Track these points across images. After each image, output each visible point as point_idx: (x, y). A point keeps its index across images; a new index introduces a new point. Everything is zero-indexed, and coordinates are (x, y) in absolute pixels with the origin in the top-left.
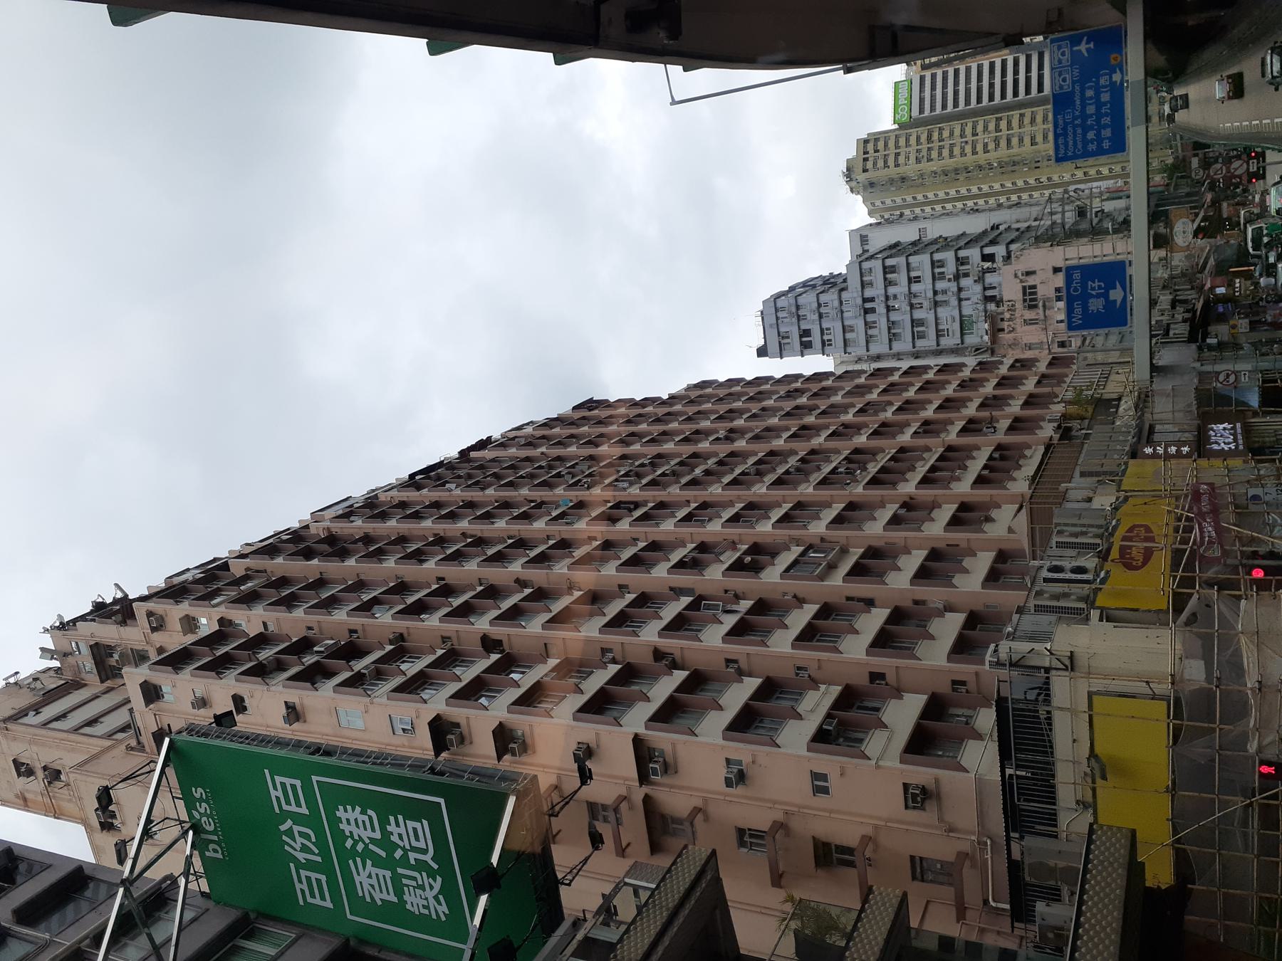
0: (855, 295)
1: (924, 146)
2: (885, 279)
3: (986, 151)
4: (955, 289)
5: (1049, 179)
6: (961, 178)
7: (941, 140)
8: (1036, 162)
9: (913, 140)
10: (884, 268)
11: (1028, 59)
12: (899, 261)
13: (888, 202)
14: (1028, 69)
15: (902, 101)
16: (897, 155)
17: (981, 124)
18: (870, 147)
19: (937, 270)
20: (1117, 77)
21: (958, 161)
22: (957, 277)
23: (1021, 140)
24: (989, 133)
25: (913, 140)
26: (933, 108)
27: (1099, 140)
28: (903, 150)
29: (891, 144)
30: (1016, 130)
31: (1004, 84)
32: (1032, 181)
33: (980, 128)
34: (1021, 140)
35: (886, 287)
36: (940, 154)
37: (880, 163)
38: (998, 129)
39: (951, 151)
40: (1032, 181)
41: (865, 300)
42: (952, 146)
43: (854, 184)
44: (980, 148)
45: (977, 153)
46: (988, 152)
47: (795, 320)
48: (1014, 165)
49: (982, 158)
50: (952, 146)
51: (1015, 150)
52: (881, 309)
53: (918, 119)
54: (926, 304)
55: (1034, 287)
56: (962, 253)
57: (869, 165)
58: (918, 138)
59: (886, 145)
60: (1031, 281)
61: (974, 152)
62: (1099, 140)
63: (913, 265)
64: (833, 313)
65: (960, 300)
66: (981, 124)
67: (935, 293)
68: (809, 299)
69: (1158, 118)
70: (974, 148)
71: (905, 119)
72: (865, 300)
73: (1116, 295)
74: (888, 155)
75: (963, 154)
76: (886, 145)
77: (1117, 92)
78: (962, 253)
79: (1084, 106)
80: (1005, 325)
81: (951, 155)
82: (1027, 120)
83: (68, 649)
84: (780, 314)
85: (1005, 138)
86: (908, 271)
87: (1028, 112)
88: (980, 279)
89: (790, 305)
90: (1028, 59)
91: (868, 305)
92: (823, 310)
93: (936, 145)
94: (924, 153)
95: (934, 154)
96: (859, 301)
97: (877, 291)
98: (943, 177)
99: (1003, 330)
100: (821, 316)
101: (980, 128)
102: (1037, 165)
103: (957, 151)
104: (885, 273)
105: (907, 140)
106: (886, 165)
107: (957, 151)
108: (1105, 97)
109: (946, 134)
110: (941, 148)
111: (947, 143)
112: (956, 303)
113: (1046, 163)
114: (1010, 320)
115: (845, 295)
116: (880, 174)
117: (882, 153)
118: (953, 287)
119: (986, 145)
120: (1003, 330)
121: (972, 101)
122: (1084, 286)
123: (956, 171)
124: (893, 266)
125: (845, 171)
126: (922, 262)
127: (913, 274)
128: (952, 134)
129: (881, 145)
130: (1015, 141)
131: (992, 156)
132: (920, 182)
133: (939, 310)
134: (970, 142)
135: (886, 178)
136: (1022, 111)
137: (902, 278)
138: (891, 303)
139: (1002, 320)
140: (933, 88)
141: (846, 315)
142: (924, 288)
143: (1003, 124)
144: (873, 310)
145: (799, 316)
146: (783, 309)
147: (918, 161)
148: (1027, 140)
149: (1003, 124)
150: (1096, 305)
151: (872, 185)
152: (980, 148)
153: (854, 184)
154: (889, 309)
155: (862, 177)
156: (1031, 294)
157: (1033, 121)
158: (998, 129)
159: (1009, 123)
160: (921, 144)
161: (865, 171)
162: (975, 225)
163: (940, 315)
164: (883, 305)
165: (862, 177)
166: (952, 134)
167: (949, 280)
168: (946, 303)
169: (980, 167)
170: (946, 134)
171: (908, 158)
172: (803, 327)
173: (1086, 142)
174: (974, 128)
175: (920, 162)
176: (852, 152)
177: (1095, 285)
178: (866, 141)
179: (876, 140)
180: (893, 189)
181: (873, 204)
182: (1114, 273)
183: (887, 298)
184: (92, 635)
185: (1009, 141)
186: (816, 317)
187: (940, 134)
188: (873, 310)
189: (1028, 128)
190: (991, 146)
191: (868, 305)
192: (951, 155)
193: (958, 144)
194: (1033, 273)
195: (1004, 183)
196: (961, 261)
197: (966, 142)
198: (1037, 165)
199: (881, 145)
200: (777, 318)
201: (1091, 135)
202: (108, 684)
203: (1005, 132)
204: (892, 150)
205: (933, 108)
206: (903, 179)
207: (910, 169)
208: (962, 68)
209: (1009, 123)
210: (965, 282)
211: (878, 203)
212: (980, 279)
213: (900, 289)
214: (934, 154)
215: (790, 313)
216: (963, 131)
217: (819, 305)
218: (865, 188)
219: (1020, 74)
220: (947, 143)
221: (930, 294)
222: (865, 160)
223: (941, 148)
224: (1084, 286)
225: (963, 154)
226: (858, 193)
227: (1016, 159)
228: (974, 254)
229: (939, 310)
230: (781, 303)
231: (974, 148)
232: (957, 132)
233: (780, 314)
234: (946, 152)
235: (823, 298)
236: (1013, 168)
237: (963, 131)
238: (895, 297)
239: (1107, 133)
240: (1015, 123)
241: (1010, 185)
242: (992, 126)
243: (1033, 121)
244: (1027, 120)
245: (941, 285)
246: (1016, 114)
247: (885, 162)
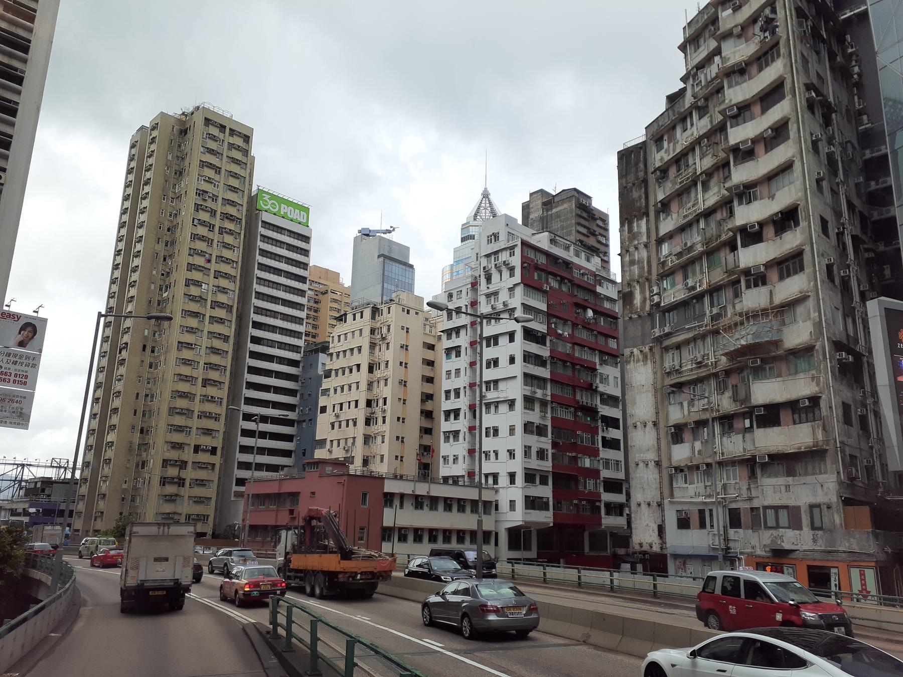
3: (189, 282)
6: (160, 247)
7: (222, 230)
8: (153, 347)
15: (284, 209)
18: (239, 141)
23: (191, 330)
24: (214, 293)
29: (235, 168)
33: (223, 283)
34: (191, 330)
36: (203, 223)
38: (216, 304)
39: (202, 238)
42: (210, 242)
44: (196, 275)
45: (189, 270)
49: (180, 276)
50: (210, 242)
51: (178, 320)
53: (257, 219)
57: (214, 131)
61: (191, 267)
69: (167, 511)
70: (198, 268)
71: (261, 204)
75: (193, 252)
81: (195, 237)
82: (218, 344)
85: (201, 310)
87: (229, 347)
94: (210, 204)
95: (204, 216)
98: (167, 224)
102: (148, 349)
103: (201, 246)
107: (201, 246)
110: (211, 227)
111: (215, 236)
113: (147, 361)
116: (196, 152)
119: (198, 284)
121: (254, 376)
128: (227, 246)
129: (238, 155)
130: (193, 322)
131: (179, 290)
134: (208, 266)
135: (188, 150)
136: (232, 340)
143: (221, 313)
147: (201, 193)
148: (189, 338)
149: (221, 313)
151: (184, 132)
152: (196, 275)
157: (215, 351)
158: (216, 304)
159: (221, 321)
166: (227, 246)
170: (229, 239)
171: (209, 181)
174: (226, 276)
178: (247, 139)
180: (170, 157)
185: (195, 315)
189: (205, 342)
192: (195, 237)
193: (209, 250)
195: (138, 273)
197: (209, 261)
198: (148, 349)
199: (238, 155)
204: (226, 166)
205: (265, 238)
206: (180, 173)
207: (192, 182)
208: (302, 314)
209: (221, 321)
214: (204, 216)
216: (227, 261)
219: (281, 322)
223: (211, 227)
231: (198, 268)
232: (227, 254)
234: (202, 231)
237: (227, 261)
240: (218, 328)
241: (133, 279)
242: (222, 298)
243: (215, 351)
244: (218, 344)
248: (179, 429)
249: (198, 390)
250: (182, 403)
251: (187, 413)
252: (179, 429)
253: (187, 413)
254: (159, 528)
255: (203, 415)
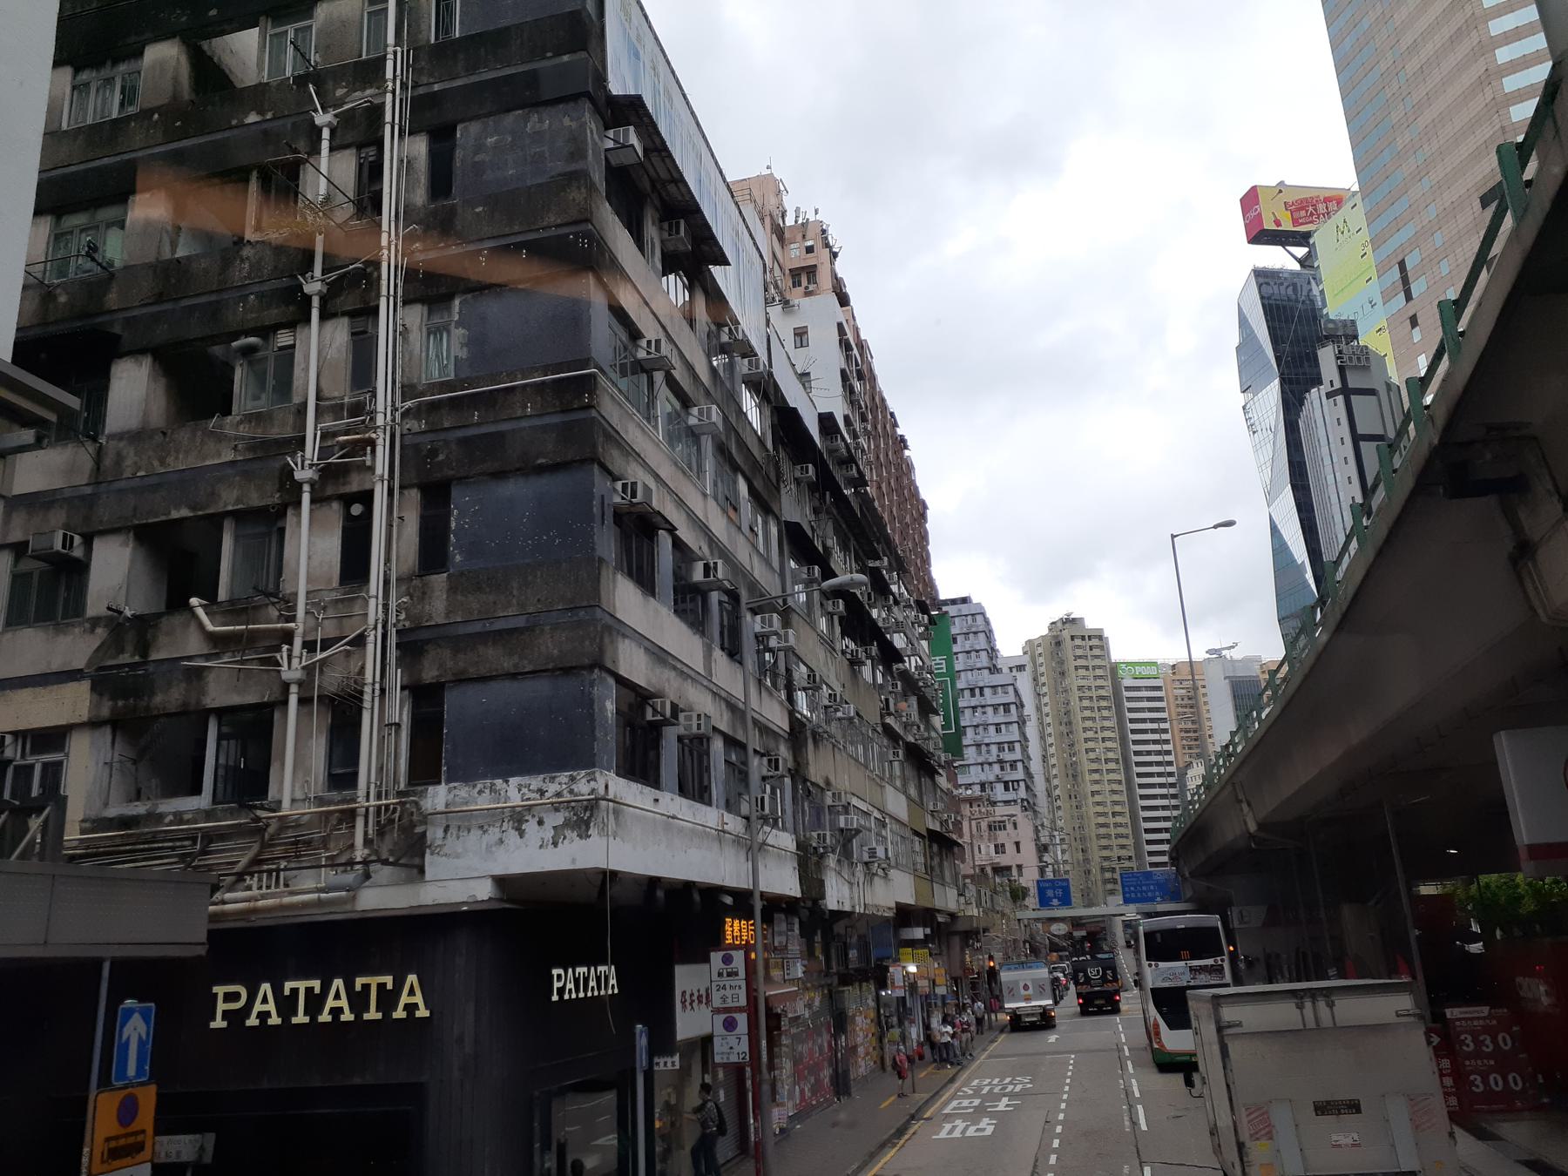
0: (986, 681)
1: (1094, 694)
2: (999, 705)
4: (990, 761)
5: (1059, 808)
6: (1063, 728)
9: (1100, 682)
10: (1009, 704)
11: (1172, 785)
12: (1014, 716)
13: (1041, 660)
14: (1161, 786)
16: (1087, 668)
17: (1113, 745)
18: (1095, 642)
19: (1006, 746)
20: (1159, 899)
21: (1079, 725)
22: (1000, 762)
23: (1097, 782)
25: (1100, 682)
26: (1129, 699)
27: (1130, 892)
28: (1091, 673)
29: (1097, 662)
30: (1107, 777)
31: (1150, 764)
32: (1057, 792)
33: (1109, 744)
34: (1097, 782)
35: (993, 705)
37: (1079, 652)
39: (1089, 719)
40: (1057, 792)
41: (981, 689)
42: (1093, 719)
43: (1060, 625)
44: (1091, 745)
46: (1087, 753)
47: (965, 630)
48: (1073, 776)
50: (1093, 719)
51: (1088, 777)
52: (974, 702)
54: (978, 738)
55: (1005, 829)
56: (1020, 765)
57: (1078, 642)
58: (1102, 687)
59: (1097, 657)
60: (1009, 827)
62: (1130, 892)
63: (1010, 727)
64: (971, 662)
65: (982, 764)
66: (1113, 745)
67: (987, 745)
68: (981, 642)
72: (981, 689)
73: (1055, 902)
74: (1087, 659)
75: (1085, 730)
76: (1097, 657)
77: (1152, 900)
78: (1020, 765)
79: (1146, 885)
80: (975, 808)
82: (1115, 787)
83: (807, 237)
84: (969, 618)
86: (1005, 723)
88: (999, 780)
89: (977, 626)
90: (1172, 785)
91: (977, 691)
92: (973, 654)
93: (1095, 705)
94: (1088, 694)
95: (1086, 703)
96: (981, 684)
97: (989, 698)
99: (971, 807)
100: (968, 652)
101: (1109, 744)
102: (1073, 797)
103: (1089, 724)
104: (1004, 705)
105: (1101, 677)
106: (1077, 657)
107: (1089, 724)
108: (1150, 894)
109: (1105, 713)
112: (980, 761)
114: (980, 812)
115: (986, 671)
117: (1089, 653)
118: (993, 758)
119: (1093, 750)
120: (971, 807)
122: (1059, 887)
123: (1069, 723)
124: (1009, 711)
125: (1072, 616)
126: (1013, 734)
127: (1003, 727)
128: (1105, 718)
129: (1096, 652)
130: (1096, 776)
131: (1084, 757)
132: (1061, 690)
133: (974, 748)
137: (1000, 718)
138: (979, 710)
139: (979, 806)
140: (1151, 710)
141: (969, 673)
142: (992, 736)
143: (1112, 766)
144: (973, 695)
145: (968, 634)
146: (974, 620)
147: (1080, 688)
148: (1096, 788)
149: (1112, 766)
150: (1050, 893)
151: (1058, 644)
152: (1091, 745)
153: (1060, 625)
154: (974, 708)
155: (1066, 634)
156: (1000, 826)
157: (1114, 792)
158: (1107, 761)
159: (1113, 771)
160: (1095, 680)
161: (1073, 638)
162: (1036, 766)
163: (970, 748)
164: (978, 704)
165: (1066, 634)
166: (1105, 718)
167: (998, 756)
168: (980, 753)
169: (1071, 745)
170: (1105, 713)
172: (959, 638)
173: (1129, 886)
174: (1110, 739)
175: (1079, 690)
176: (1090, 624)
177: (1060, 892)
178: (1100, 637)
179: (1102, 648)
181: (1039, 645)
182: (1066, 901)
183: (983, 707)
184: (822, 263)
185: (1096, 771)
186: (968, 649)
187: (1106, 708)
188: (973, 695)
189: (1108, 788)
190: (1092, 755)
191: (977, 691)
194: (1016, 828)
196: (1013, 765)
197: (1096, 732)
200: (966, 616)
201: (1132, 888)
202: (787, 272)
203: (1105, 767)
204: (1091, 663)
205: (1129, 699)
206: (1063, 674)
207: (1074, 681)
209: (1113, 771)
210: (996, 767)
211: (1040, 650)
212: (999, 780)
213: (991, 717)
214: (1086, 703)
215: (971, 626)
216: (1108, 729)
217: (977, 651)
218: (1055, 637)
220: (1096, 714)
221: (987, 741)
222: (1083, 638)
223: (1092, 709)
224: (1059, 887)
225: (1085, 730)
226: (1050, 630)
227: (1080, 779)
228: (1019, 774)
229: (974, 748)
230: (979, 618)
232: (1107, 724)
233: (969, 618)
234: (1087, 713)
235: (983, 654)
236: (1070, 776)
237: (1108, 729)
238: (984, 713)
239: (1133, 895)
242: (1111, 755)
243: (1114, 792)
244: (1115, 787)
245: (994, 749)
246: (1121, 777)
247: (1080, 657)
248: (1105, 848)
249: (1111, 820)
250: (1102, 831)
251: (1108, 836)
252: (1105, 848)
253: (1108, 836)
254: (1300, 1007)
255: (1118, 836)
